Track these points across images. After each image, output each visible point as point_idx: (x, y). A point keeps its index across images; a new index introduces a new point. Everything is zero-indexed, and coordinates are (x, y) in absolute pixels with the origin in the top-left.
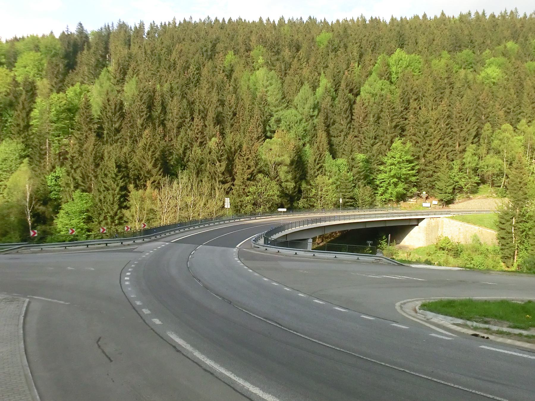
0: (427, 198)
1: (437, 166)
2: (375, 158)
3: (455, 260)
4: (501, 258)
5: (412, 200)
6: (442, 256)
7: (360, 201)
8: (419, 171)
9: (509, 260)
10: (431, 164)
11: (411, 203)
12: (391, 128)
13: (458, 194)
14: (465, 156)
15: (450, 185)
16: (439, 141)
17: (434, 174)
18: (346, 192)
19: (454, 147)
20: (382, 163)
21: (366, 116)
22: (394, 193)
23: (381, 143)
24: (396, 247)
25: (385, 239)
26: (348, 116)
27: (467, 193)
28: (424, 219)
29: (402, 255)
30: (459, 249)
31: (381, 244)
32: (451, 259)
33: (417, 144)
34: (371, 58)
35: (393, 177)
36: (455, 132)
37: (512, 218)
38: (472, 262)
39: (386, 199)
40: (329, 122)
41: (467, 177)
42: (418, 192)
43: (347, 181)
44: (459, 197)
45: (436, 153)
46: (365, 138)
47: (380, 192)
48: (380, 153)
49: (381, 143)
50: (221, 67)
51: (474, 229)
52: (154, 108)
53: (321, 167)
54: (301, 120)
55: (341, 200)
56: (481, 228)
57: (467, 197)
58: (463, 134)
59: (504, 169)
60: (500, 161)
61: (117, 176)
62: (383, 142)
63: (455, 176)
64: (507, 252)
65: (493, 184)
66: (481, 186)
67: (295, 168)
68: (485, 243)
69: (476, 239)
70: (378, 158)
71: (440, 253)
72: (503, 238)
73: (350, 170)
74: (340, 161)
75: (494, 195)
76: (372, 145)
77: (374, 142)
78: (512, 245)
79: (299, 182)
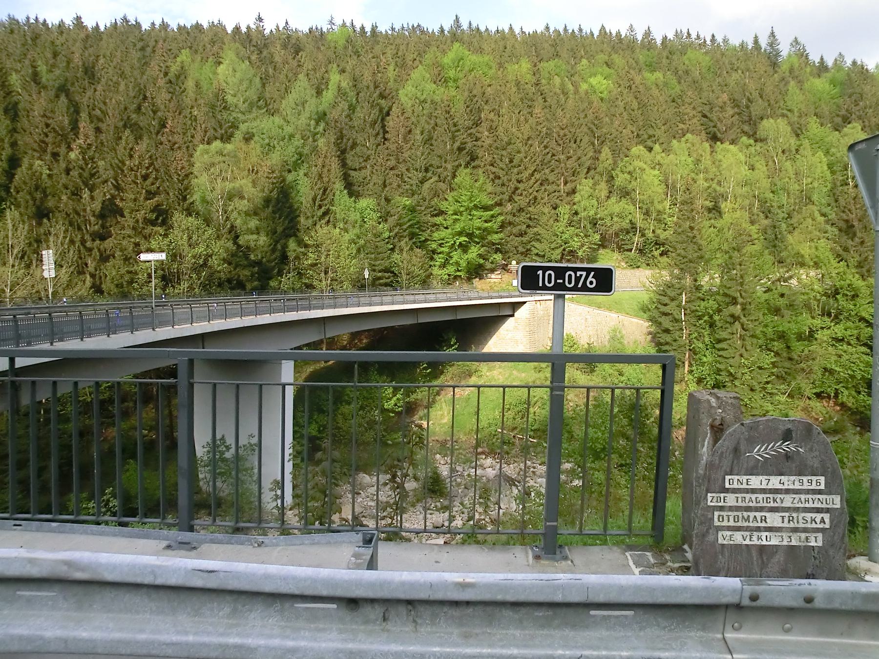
2: (426, 203)
5: (493, 276)
7: (404, 277)
8: (502, 226)
14: (576, 200)
15: (557, 248)
16: (532, 175)
18: (376, 259)
20: (441, 213)
21: (410, 131)
22: (463, 264)
25: (455, 344)
26: (378, 134)
28: (525, 303)
29: (488, 374)
33: (497, 181)
35: (460, 234)
36: (558, 161)
37: (681, 294)
39: (449, 275)
42: (504, 262)
43: (378, 239)
45: (530, 194)
48: (436, 195)
50: (161, 67)
53: (325, 214)
54: (291, 136)
55: (366, 274)
60: (632, 208)
62: (439, 177)
67: (274, 212)
69: (615, 336)
70: (433, 203)
73: (384, 219)
74: (363, 203)
75: (623, 264)
76: (422, 183)
77: (425, 177)
78: (682, 343)
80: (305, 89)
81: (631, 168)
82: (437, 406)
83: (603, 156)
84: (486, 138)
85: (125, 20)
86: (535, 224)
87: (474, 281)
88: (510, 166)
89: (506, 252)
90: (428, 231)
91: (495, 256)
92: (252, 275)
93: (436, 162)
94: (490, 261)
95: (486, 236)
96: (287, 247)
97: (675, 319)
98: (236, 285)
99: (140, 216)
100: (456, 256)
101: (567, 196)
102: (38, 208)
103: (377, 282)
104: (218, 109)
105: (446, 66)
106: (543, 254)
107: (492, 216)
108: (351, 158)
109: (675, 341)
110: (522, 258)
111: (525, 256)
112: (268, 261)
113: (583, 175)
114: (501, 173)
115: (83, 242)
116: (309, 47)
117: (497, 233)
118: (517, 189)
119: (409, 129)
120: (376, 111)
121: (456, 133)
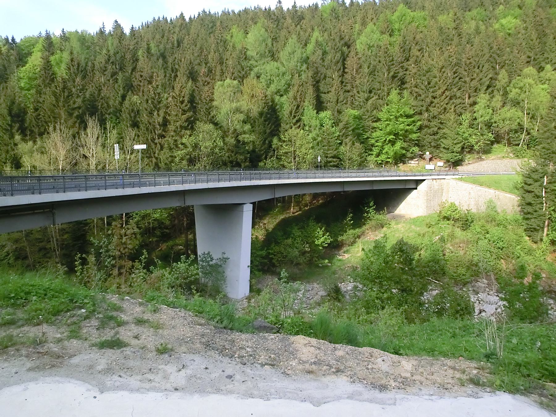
0: (431, 159)
1: (442, 122)
2: (369, 114)
3: (464, 233)
4: (525, 230)
5: (412, 162)
6: (446, 228)
8: (420, 128)
9: (536, 234)
10: (436, 120)
11: (412, 165)
12: (388, 79)
13: (467, 155)
15: (458, 143)
16: (444, 92)
17: (439, 131)
19: (464, 100)
20: (378, 120)
23: (377, 97)
24: (388, 216)
25: (374, 206)
26: (340, 69)
27: (478, 153)
28: (424, 180)
29: (395, 226)
30: (469, 218)
31: (368, 213)
32: (458, 232)
33: (418, 98)
34: (373, 17)
35: (390, 134)
36: (465, 82)
38: (487, 236)
39: (383, 161)
40: (320, 77)
41: (479, 134)
42: (420, 153)
44: (469, 158)
46: (358, 92)
47: (375, 153)
49: (377, 97)
51: (490, 193)
52: (124, 69)
53: (298, 121)
54: (284, 74)
56: (497, 192)
57: (478, 158)
58: (474, 83)
59: (524, 123)
60: (520, 114)
61: (11, 126)
62: (379, 96)
63: (464, 133)
64: (534, 223)
65: (509, 144)
66: (495, 146)
67: (265, 121)
68: (503, 211)
69: (491, 205)
70: (373, 114)
71: (444, 224)
72: (529, 204)
75: (511, 155)
76: (367, 100)
77: (369, 96)
79: (269, 139)
80: (295, 44)
81: (522, 84)
82: (356, 245)
83: (500, 77)
84: (413, 69)
85: (204, 11)
86: (444, 127)
87: (399, 165)
88: (428, 87)
89: (423, 146)
90: (370, 132)
91: (414, 149)
92: (246, 159)
93: (377, 86)
94: (410, 152)
95: (408, 135)
96: (272, 142)
97: (536, 195)
98: (235, 165)
99: (178, 124)
100: (387, 148)
101: (470, 107)
102: (133, 121)
103: (328, 165)
104: (242, 59)
105: (393, 22)
106: (448, 147)
107: (414, 122)
108: (323, 86)
109: (536, 211)
110: (434, 150)
111: (437, 149)
112: (259, 151)
113: (483, 91)
114: (421, 92)
115: (153, 140)
116: (308, 16)
117: (416, 133)
118: (432, 103)
119: (359, 65)
120: (339, 55)
121: (392, 67)
